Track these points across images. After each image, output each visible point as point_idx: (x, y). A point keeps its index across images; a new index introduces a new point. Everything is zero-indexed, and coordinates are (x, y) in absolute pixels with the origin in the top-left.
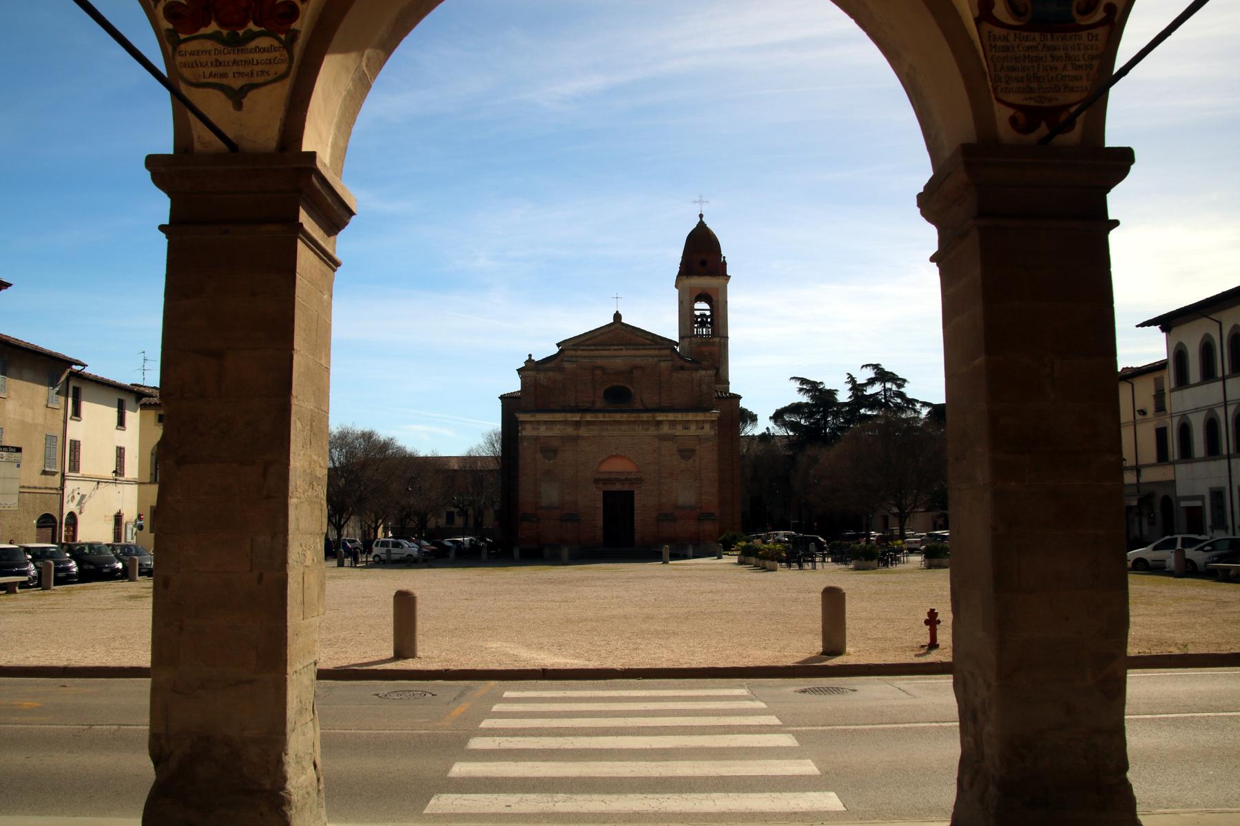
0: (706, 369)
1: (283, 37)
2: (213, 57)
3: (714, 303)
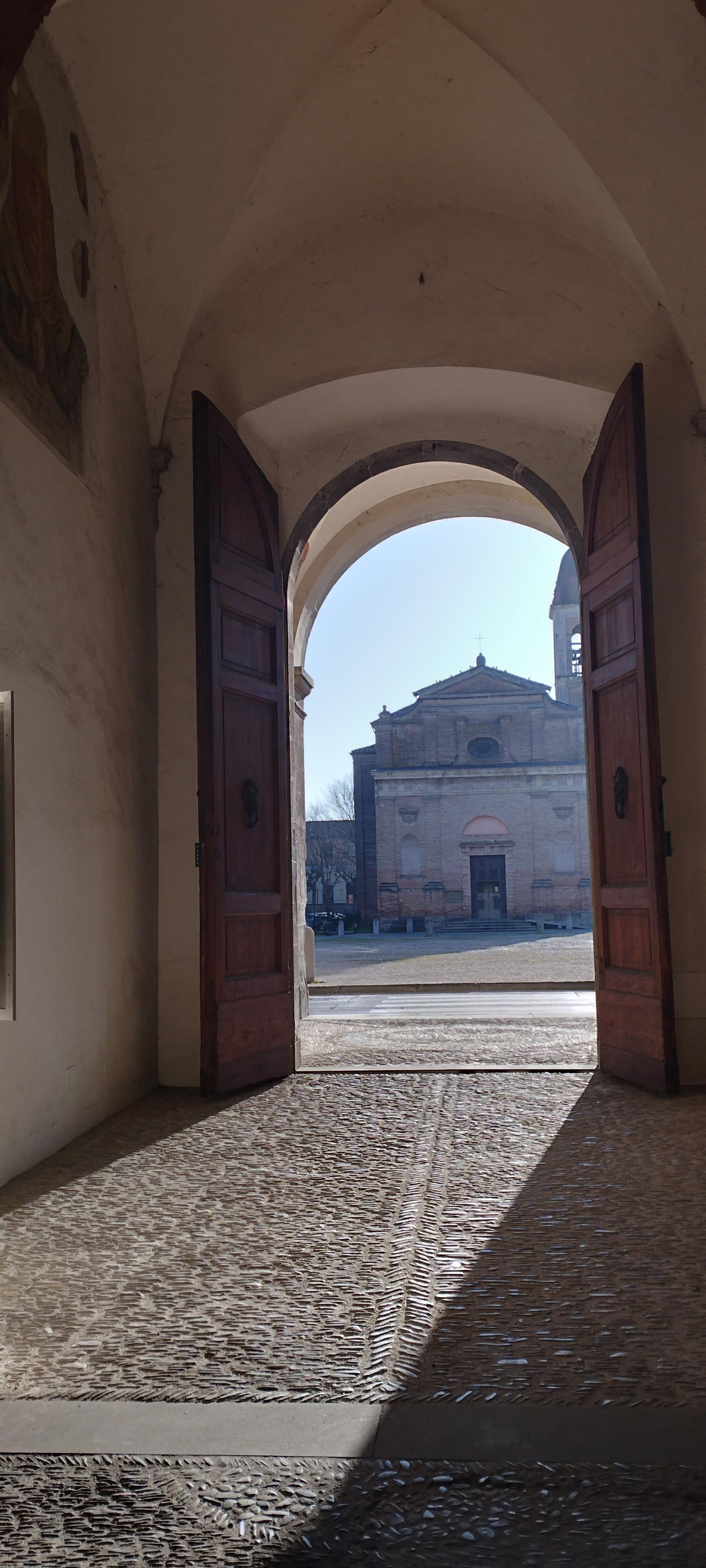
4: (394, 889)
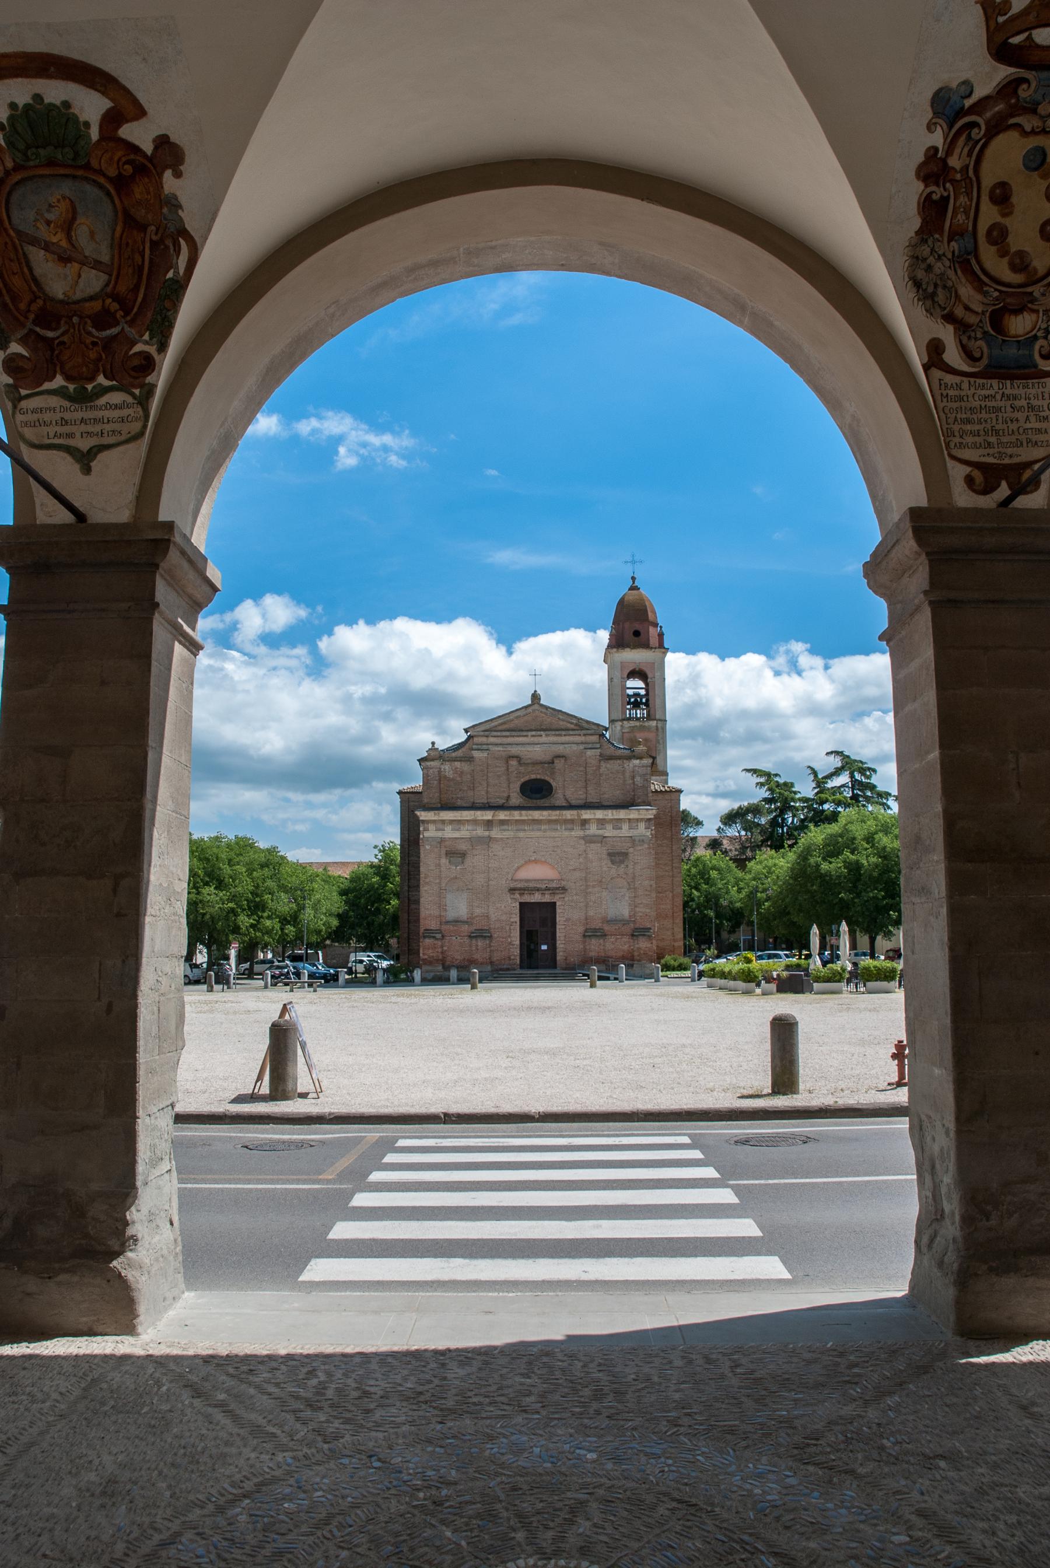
0: (641, 758)
1: (137, 392)
2: (58, 416)
3: (649, 680)
4: (439, 936)
